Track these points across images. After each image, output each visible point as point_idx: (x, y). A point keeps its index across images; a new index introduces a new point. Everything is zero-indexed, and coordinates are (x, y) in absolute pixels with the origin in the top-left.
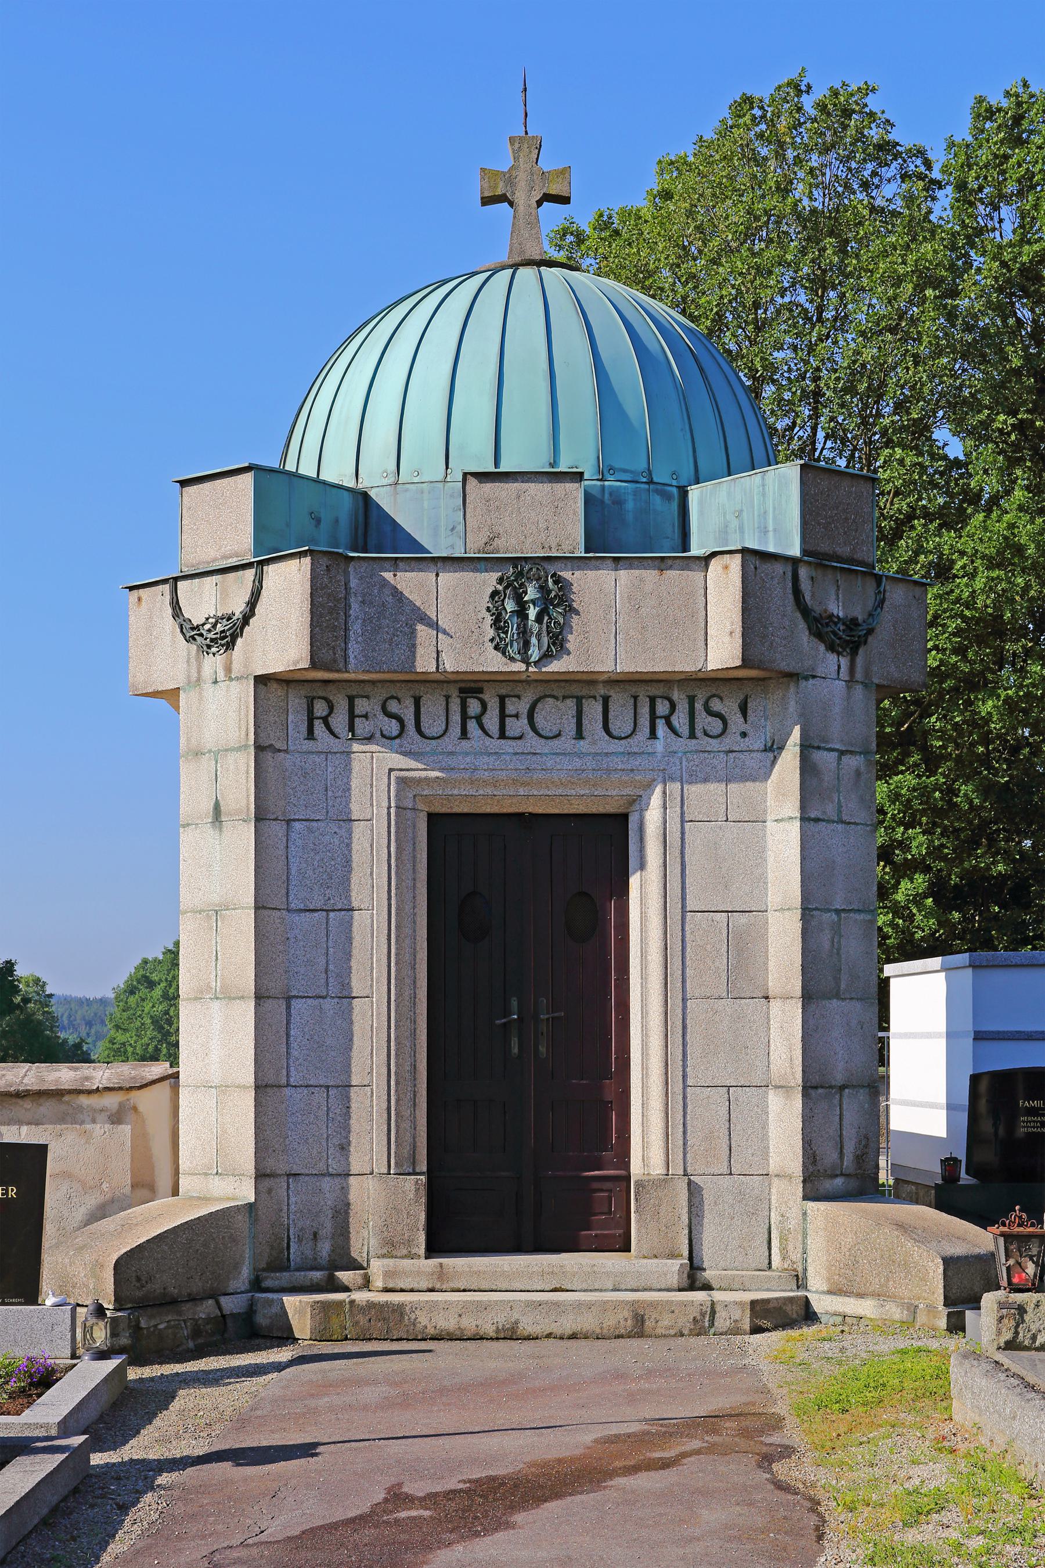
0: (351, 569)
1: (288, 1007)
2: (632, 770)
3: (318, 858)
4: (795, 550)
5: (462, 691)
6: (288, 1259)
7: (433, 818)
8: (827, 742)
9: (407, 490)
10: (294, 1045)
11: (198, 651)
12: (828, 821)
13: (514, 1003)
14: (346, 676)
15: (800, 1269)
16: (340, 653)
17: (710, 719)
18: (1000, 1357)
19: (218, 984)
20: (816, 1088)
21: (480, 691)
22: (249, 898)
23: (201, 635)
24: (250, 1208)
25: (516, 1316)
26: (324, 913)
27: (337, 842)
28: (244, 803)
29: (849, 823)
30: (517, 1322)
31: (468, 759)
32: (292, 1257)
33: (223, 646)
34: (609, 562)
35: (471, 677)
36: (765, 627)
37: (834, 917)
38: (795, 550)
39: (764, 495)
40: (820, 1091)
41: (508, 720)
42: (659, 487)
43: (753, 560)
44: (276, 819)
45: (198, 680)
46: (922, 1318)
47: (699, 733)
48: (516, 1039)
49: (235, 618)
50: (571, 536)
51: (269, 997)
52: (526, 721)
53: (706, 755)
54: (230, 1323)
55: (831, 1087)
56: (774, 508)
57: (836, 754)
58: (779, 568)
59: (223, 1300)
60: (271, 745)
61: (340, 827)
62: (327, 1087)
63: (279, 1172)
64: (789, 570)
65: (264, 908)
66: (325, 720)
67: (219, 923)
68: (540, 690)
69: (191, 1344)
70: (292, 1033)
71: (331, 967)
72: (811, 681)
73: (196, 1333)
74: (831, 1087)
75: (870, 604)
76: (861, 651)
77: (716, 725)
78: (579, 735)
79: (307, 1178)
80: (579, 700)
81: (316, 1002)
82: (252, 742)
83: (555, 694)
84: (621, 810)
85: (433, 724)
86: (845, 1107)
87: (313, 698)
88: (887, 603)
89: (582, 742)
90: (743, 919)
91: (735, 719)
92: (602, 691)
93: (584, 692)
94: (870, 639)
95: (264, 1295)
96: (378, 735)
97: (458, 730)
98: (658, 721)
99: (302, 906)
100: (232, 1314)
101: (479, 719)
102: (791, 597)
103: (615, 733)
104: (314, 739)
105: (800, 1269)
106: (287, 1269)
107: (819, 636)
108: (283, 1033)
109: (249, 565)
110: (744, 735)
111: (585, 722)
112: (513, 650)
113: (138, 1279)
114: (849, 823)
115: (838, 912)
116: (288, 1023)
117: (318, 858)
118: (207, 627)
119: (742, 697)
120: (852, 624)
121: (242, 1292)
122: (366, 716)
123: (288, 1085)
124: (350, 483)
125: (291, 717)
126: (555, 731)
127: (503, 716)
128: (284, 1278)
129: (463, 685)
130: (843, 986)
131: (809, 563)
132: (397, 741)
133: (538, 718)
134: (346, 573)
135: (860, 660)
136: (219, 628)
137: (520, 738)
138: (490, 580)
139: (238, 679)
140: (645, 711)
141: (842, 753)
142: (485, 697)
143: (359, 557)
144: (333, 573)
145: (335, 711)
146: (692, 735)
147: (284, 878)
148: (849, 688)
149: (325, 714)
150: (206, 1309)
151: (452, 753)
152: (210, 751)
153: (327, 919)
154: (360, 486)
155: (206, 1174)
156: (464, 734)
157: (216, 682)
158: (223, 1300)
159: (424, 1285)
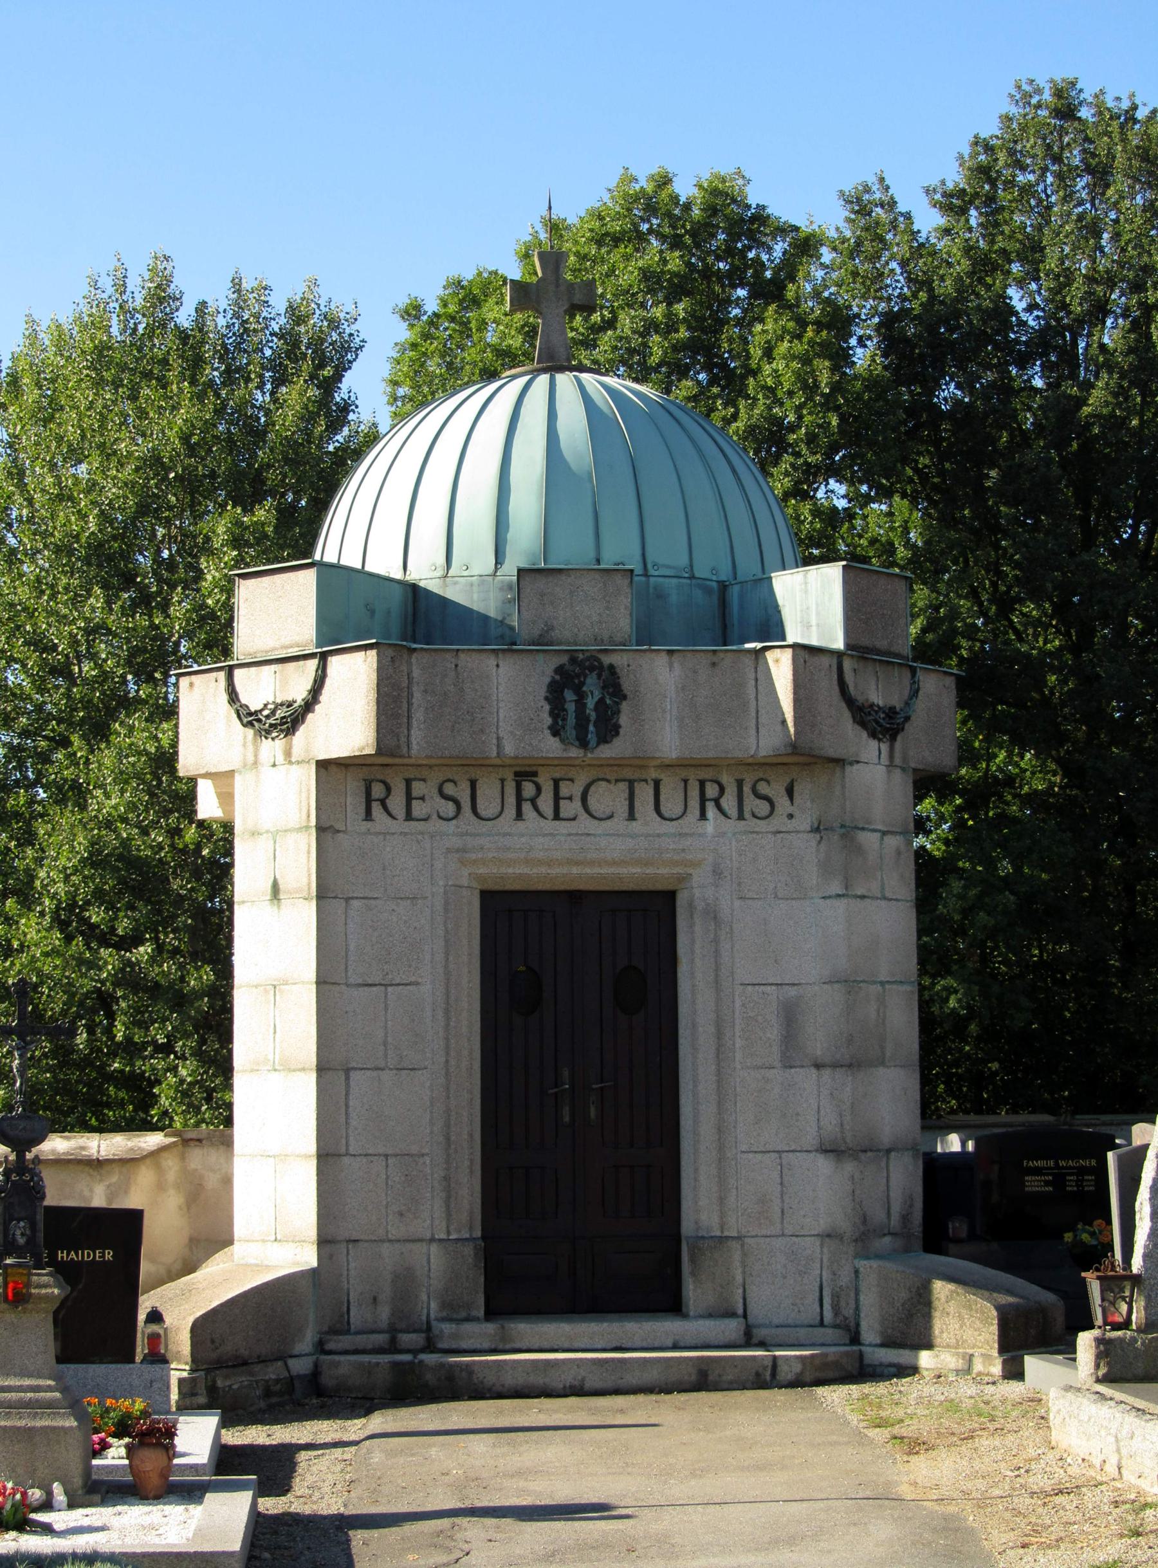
0: (414, 660)
1: (347, 1078)
2: (683, 850)
3: (376, 934)
4: (839, 644)
5: (517, 774)
6: (348, 1323)
7: (488, 897)
8: (869, 823)
9: (456, 583)
10: (353, 1115)
11: (255, 735)
12: (872, 898)
13: (566, 1073)
14: (406, 761)
15: (852, 1324)
16: (403, 739)
17: (758, 801)
18: (1100, 1388)
19: (277, 1057)
20: (865, 1151)
21: (535, 774)
22: (309, 970)
23: (259, 721)
24: (313, 1272)
25: (583, 1373)
26: (383, 988)
27: (395, 919)
28: (305, 881)
29: (891, 900)
30: (583, 1380)
31: (523, 840)
32: (352, 1320)
33: (282, 731)
34: (664, 654)
35: (527, 762)
36: (814, 716)
37: (880, 988)
38: (839, 644)
39: (806, 592)
40: (869, 1154)
41: (562, 802)
42: (699, 581)
43: (801, 653)
44: (335, 898)
45: (255, 763)
46: (978, 1366)
47: (747, 815)
48: (567, 1108)
49: (296, 705)
50: (623, 623)
51: (329, 1069)
52: (579, 804)
53: (754, 835)
54: (297, 1384)
55: (879, 1150)
56: (817, 605)
57: (878, 835)
58: (825, 661)
59: (291, 1362)
60: (331, 827)
61: (398, 905)
62: (386, 1156)
63: (339, 1238)
64: (835, 661)
65: (325, 982)
66: (383, 802)
67: (278, 997)
68: (594, 773)
69: (262, 1404)
70: (351, 1103)
71: (390, 1039)
72: (856, 767)
73: (268, 1393)
74: (879, 1150)
75: (906, 693)
76: (899, 738)
77: (763, 808)
78: (632, 816)
79: (366, 1245)
80: (631, 783)
81: (375, 1073)
82: (313, 822)
83: (608, 777)
84: (670, 888)
85: (488, 806)
86: (891, 1168)
87: (371, 782)
88: (921, 693)
89: (634, 823)
90: (793, 992)
91: (782, 802)
92: (654, 774)
93: (636, 776)
94: (907, 726)
95: (330, 1357)
96: (435, 816)
97: (514, 812)
98: (707, 803)
99: (360, 981)
100: (299, 1376)
101: (533, 801)
102: (837, 688)
103: (666, 815)
104: (371, 820)
105: (852, 1324)
106: (348, 1332)
107: (862, 724)
108: (342, 1104)
109: (311, 656)
110: (791, 816)
111: (637, 804)
112: (570, 732)
113: (213, 1342)
114: (891, 900)
115: (882, 983)
116: (347, 1094)
117: (376, 934)
118: (266, 713)
119: (789, 780)
120: (891, 712)
121: (306, 1355)
122: (422, 798)
123: (347, 1154)
124: (397, 574)
125: (349, 800)
126: (608, 812)
127: (557, 798)
128: (345, 1342)
129: (518, 769)
130: (888, 1054)
131: (852, 656)
132: (454, 822)
133: (592, 801)
134: (410, 664)
135: (898, 745)
136: (280, 714)
137: (574, 819)
138: (543, 670)
139: (298, 762)
140: (694, 793)
141: (884, 833)
142: (538, 780)
143: (422, 649)
144: (397, 664)
145: (393, 793)
146: (741, 817)
147: (343, 954)
148: (889, 772)
149: (382, 796)
150: (273, 1372)
151: (505, 835)
152: (267, 832)
153: (386, 994)
154: (408, 578)
155: (263, 1241)
156: (519, 815)
157: (274, 765)
158: (291, 1362)
159: (486, 1345)
